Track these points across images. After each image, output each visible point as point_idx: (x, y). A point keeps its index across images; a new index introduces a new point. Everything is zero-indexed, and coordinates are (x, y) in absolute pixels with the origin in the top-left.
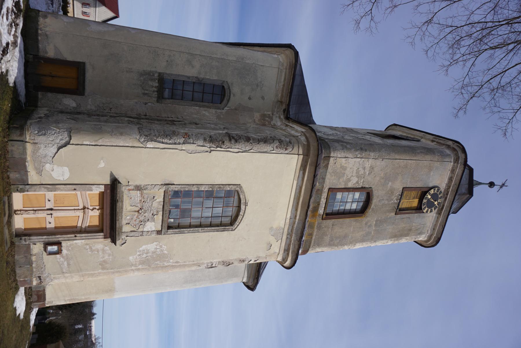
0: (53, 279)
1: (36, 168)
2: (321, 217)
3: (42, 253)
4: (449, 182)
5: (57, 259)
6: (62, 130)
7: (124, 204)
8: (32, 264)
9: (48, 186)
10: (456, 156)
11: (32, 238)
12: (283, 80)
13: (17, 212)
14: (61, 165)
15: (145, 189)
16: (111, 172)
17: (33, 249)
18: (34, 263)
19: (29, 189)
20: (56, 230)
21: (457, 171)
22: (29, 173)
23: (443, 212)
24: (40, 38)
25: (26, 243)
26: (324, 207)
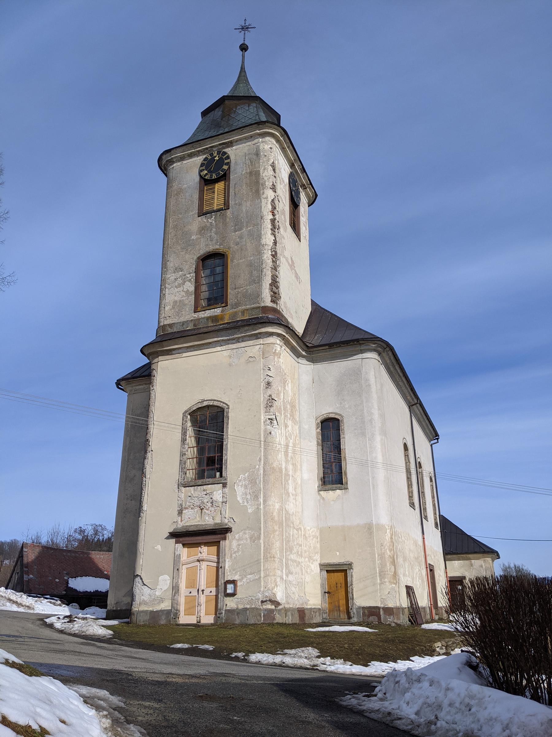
0: (267, 588)
1: (159, 603)
3: (236, 599)
8: (246, 608)
9: (173, 593)
10: (168, 164)
12: (140, 387)
14: (157, 583)
18: (245, 607)
19: (175, 609)
21: (179, 155)
22: (163, 609)
23: (227, 141)
24: (119, 609)
25: (224, 613)
26: (213, 310)
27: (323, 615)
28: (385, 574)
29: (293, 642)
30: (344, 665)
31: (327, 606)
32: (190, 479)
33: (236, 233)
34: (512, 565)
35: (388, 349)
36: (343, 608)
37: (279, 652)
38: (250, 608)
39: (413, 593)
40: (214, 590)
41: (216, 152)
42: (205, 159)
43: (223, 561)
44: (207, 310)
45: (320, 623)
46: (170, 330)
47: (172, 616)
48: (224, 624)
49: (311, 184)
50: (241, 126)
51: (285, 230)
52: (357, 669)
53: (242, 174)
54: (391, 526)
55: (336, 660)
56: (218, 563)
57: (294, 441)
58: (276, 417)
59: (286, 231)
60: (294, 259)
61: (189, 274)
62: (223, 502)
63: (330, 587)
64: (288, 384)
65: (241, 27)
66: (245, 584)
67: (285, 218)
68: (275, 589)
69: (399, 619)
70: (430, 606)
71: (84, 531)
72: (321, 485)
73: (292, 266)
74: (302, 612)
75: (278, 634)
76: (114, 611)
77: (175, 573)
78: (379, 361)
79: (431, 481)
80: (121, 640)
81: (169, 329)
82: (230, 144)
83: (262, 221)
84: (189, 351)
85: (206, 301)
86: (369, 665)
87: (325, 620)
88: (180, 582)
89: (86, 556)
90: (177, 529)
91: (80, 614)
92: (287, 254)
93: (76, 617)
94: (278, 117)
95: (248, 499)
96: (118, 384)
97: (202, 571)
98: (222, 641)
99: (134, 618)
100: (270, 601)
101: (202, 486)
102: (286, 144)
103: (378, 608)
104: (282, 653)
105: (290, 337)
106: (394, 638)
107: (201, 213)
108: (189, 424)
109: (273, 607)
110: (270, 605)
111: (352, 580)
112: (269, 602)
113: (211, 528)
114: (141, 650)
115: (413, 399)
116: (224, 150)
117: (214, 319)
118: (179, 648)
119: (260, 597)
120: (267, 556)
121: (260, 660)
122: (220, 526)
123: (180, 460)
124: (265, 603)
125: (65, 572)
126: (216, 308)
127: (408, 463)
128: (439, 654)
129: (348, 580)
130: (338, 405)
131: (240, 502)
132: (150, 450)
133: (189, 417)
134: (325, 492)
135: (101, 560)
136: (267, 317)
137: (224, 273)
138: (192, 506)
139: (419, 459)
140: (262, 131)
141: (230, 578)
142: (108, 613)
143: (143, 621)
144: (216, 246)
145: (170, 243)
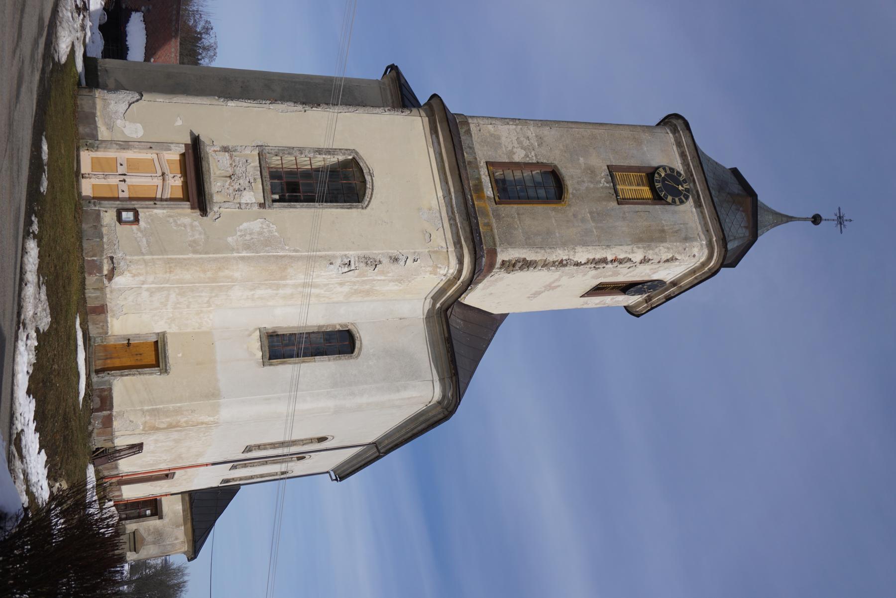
0: (130, 264)
2: (493, 200)
4: (684, 160)
7: (211, 167)
12: (389, 97)
15: (234, 151)
16: (191, 131)
17: (104, 218)
19: (99, 145)
21: (684, 140)
22: (98, 129)
23: (702, 200)
24: (99, 73)
26: (490, 186)
27: (100, 338)
28: (155, 415)
29: (57, 298)
30: (28, 363)
31: (112, 343)
32: (269, 161)
33: (588, 215)
34: (186, 578)
35: (446, 413)
36: (110, 363)
37: (41, 279)
38: (103, 242)
39: (134, 452)
40: (126, 195)
41: (688, 187)
42: (679, 174)
43: (164, 206)
44: (490, 177)
45: (89, 334)
46: (462, 131)
47: (90, 141)
48: (81, 208)
49: (652, 308)
50: (721, 217)
51: (594, 277)
52: (22, 381)
53: (662, 219)
54: (217, 423)
55: (34, 353)
56: (161, 200)
57: (323, 295)
58: (353, 270)
59: (592, 278)
60: (559, 289)
61: (536, 155)
62: (240, 205)
63: (137, 346)
64: (397, 285)
65: (842, 215)
66: (134, 235)
67: (610, 276)
68: (129, 275)
69: (99, 435)
70: (121, 475)
71: (207, 34)
72: (267, 331)
73: (550, 287)
74: (101, 310)
75: (69, 278)
76: (96, 67)
77: (146, 144)
78: (430, 402)
79: (283, 473)
80: (52, 72)
81: (464, 130)
82: (698, 204)
83: (604, 247)
84: (436, 156)
85: (502, 177)
86: (29, 397)
87: (93, 340)
88: (135, 150)
89: (173, 34)
90: (204, 146)
91: (91, 23)
92: (565, 280)
93: (84, 17)
94: (733, 265)
95: (245, 236)
96: (393, 68)
97: (149, 179)
98: (55, 205)
99: (85, 92)
100: (113, 269)
101: (260, 176)
102: (700, 275)
103: (111, 408)
104: (41, 282)
105: (458, 286)
106: (71, 429)
107: (611, 170)
108: (341, 158)
109: (105, 272)
110: (107, 268)
111: (146, 374)
112: (112, 266)
113: (206, 189)
114: (35, 96)
115: (384, 447)
116: (691, 196)
117: (479, 188)
118: (41, 147)
119: (118, 255)
121: (28, 254)
122: (209, 201)
123: (294, 148)
124: (110, 262)
125: (151, 7)
126: (493, 190)
127: (302, 444)
128: (51, 487)
129: (146, 369)
130: (372, 351)
131: (241, 226)
132: (306, 109)
133: (350, 157)
134: (259, 337)
135: (169, 54)
136: (482, 256)
137: (538, 200)
138: (234, 164)
139: (309, 457)
140: (715, 244)
141: (141, 215)
142: (94, 60)
143: (81, 104)
144: (571, 189)
145: (573, 130)
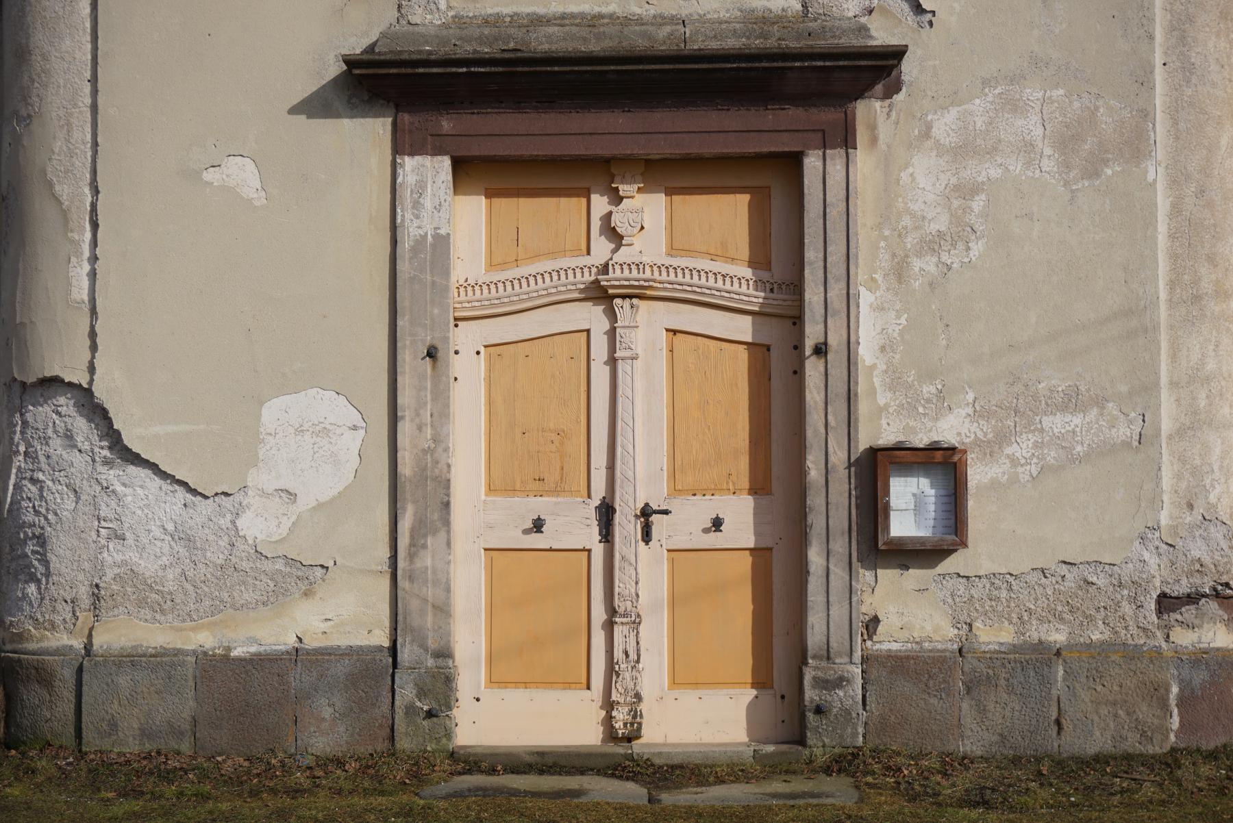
0: (1199, 510)
3: (950, 583)
5: (1014, 480)
6: (17, 437)
8: (1040, 646)
9: (405, 524)
11: (815, 638)
13: (618, 725)
20: (776, 486)
22: (311, 643)
38: (1070, 647)
120: (1196, 281)
124: (1188, 612)
